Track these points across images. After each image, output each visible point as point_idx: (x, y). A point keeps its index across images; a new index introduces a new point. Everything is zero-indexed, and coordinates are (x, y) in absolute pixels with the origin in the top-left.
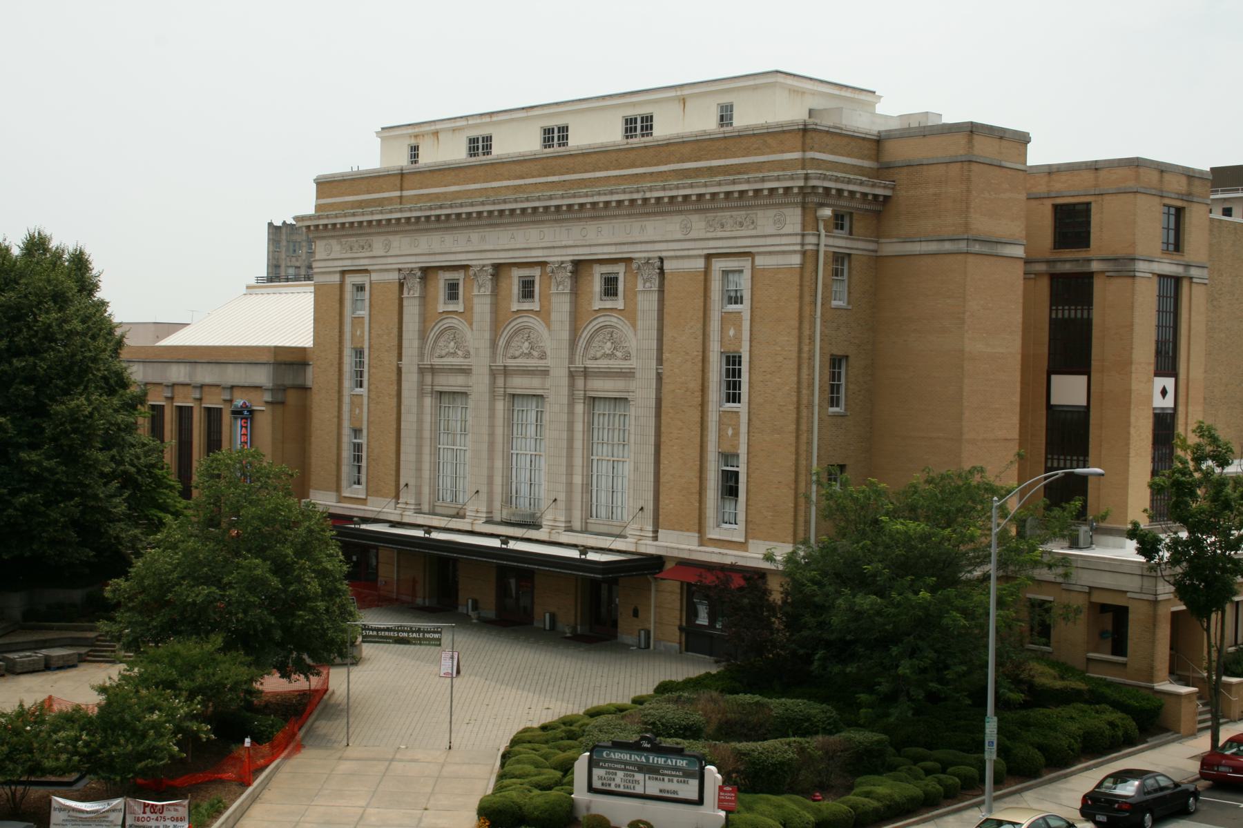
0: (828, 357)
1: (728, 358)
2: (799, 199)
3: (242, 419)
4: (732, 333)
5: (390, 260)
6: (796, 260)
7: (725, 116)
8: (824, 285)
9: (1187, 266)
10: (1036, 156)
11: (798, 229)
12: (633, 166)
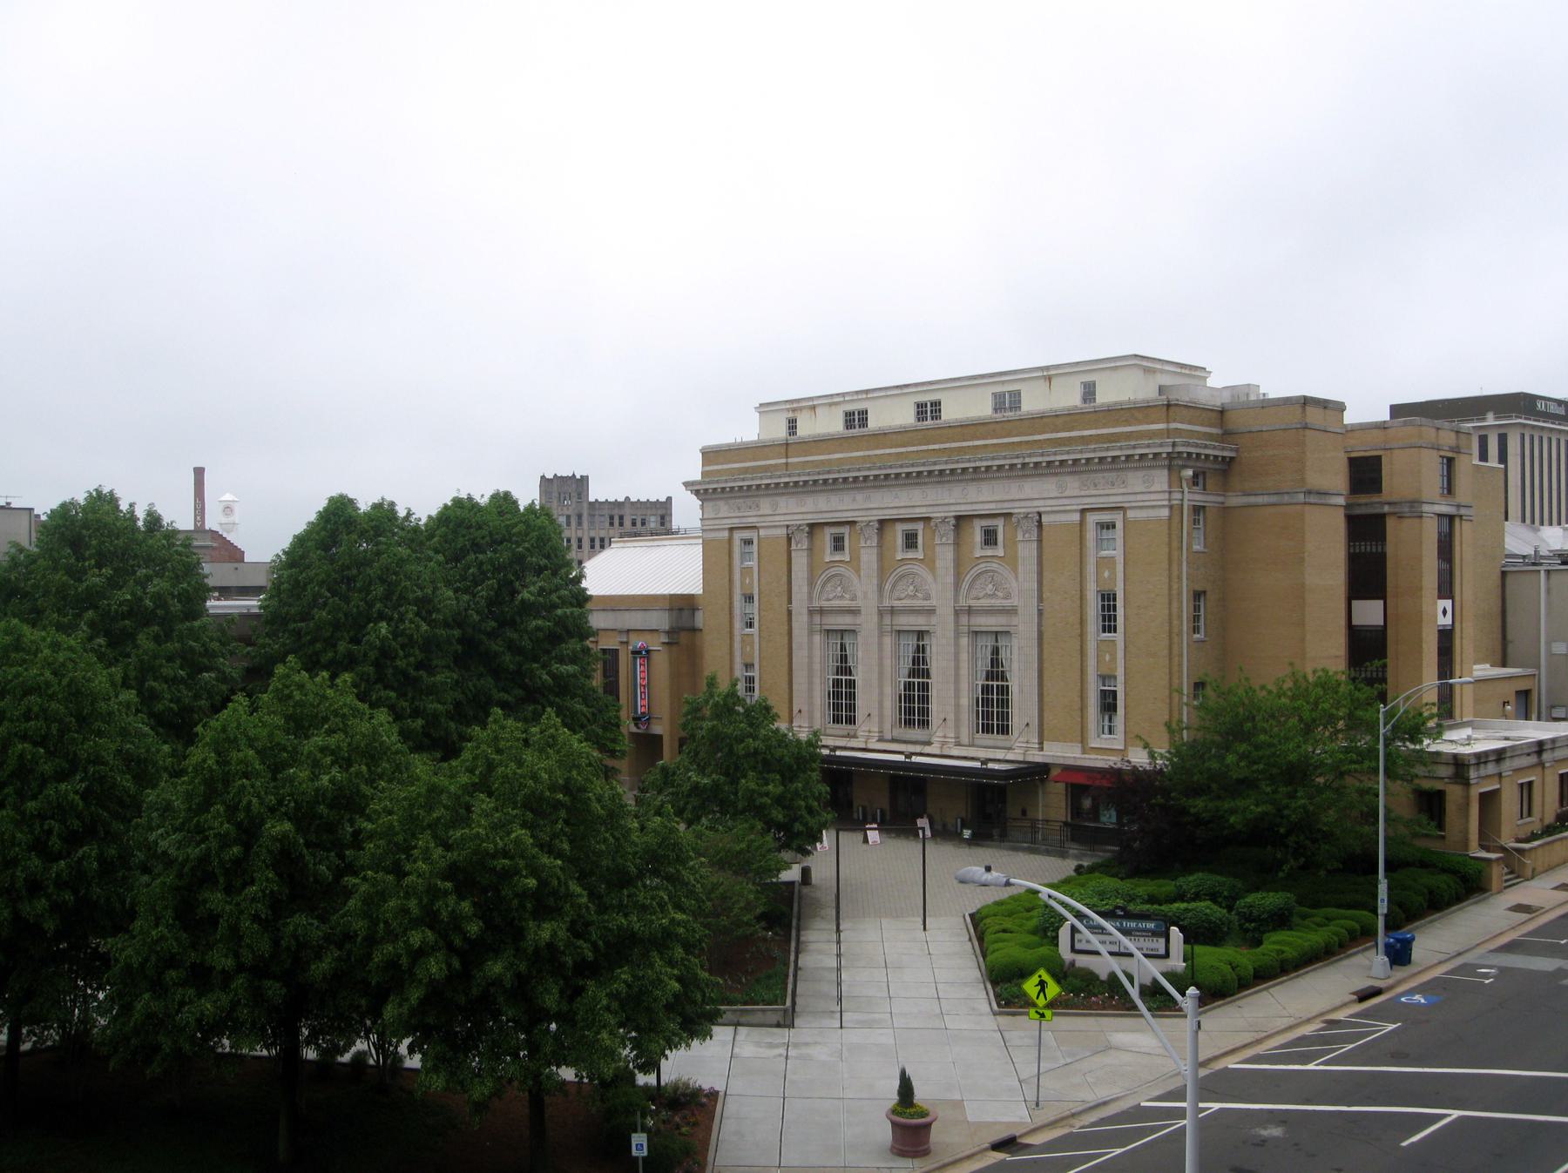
1: (1103, 596)
2: (1166, 463)
4: (1106, 574)
5: (777, 518)
6: (1165, 513)
7: (1089, 391)
8: (1188, 533)
9: (1458, 506)
10: (1350, 418)
11: (1166, 487)
12: (1008, 435)
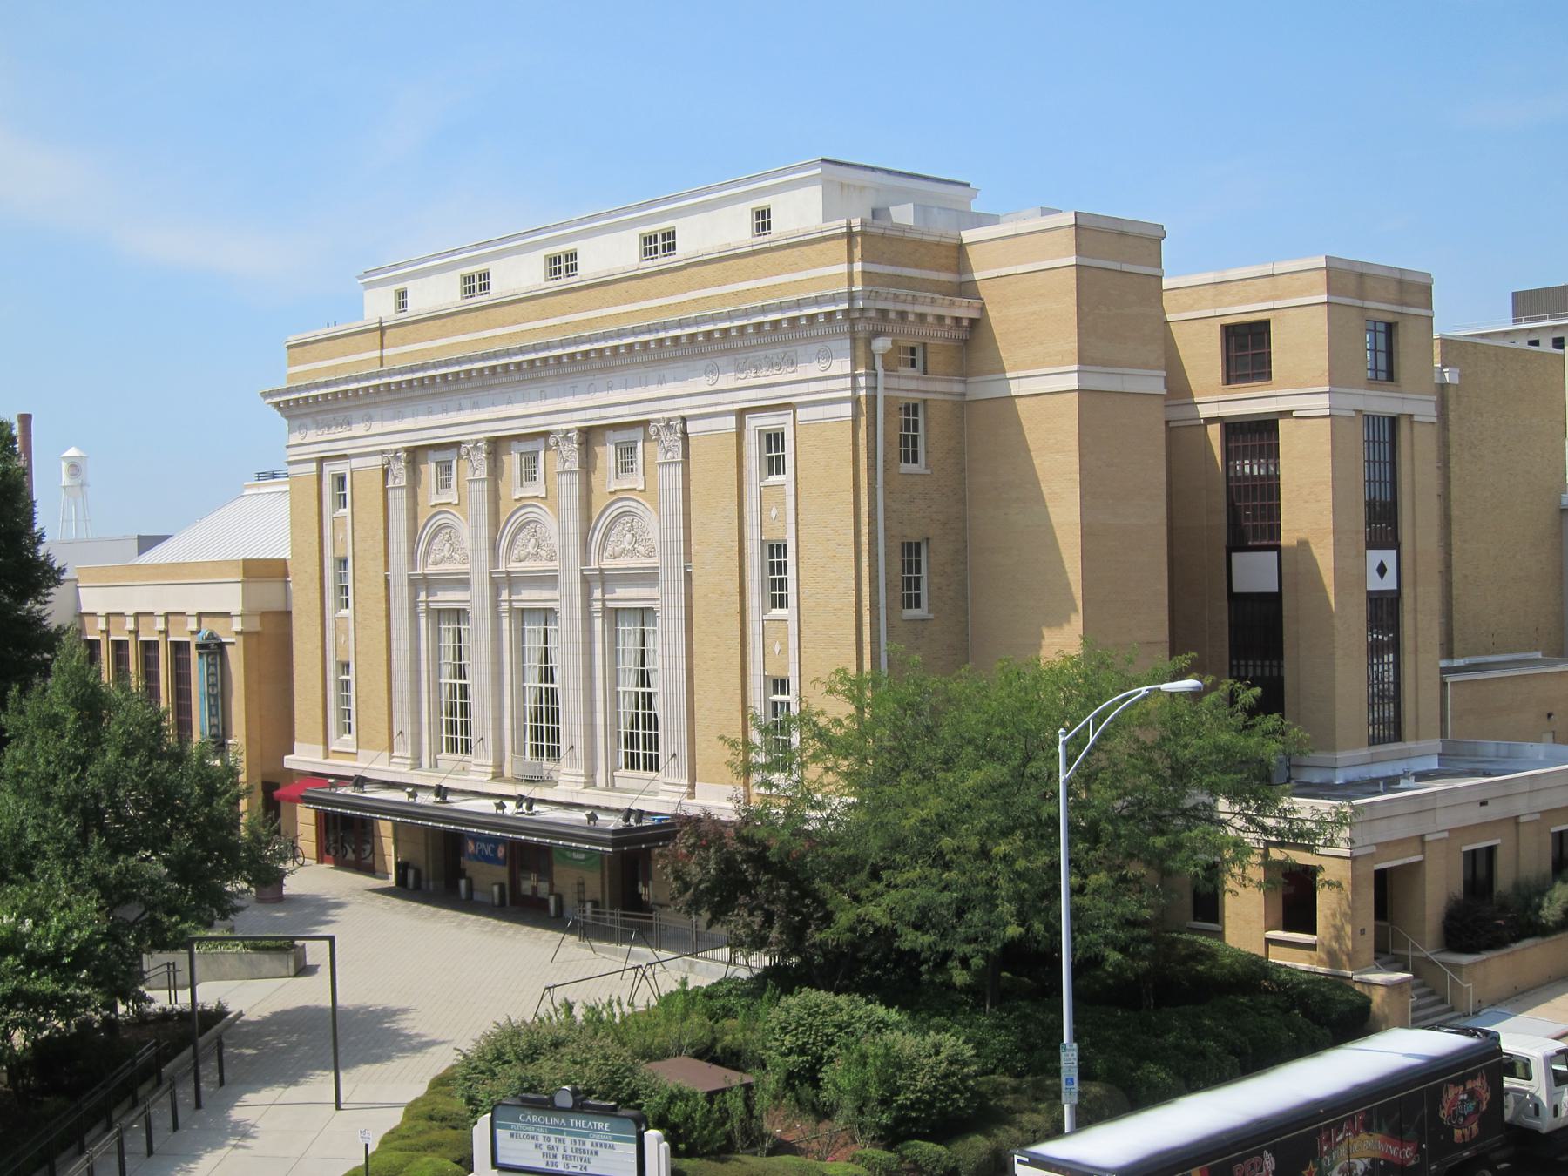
0: (897, 543)
2: (846, 327)
3: (208, 655)
6: (847, 409)
